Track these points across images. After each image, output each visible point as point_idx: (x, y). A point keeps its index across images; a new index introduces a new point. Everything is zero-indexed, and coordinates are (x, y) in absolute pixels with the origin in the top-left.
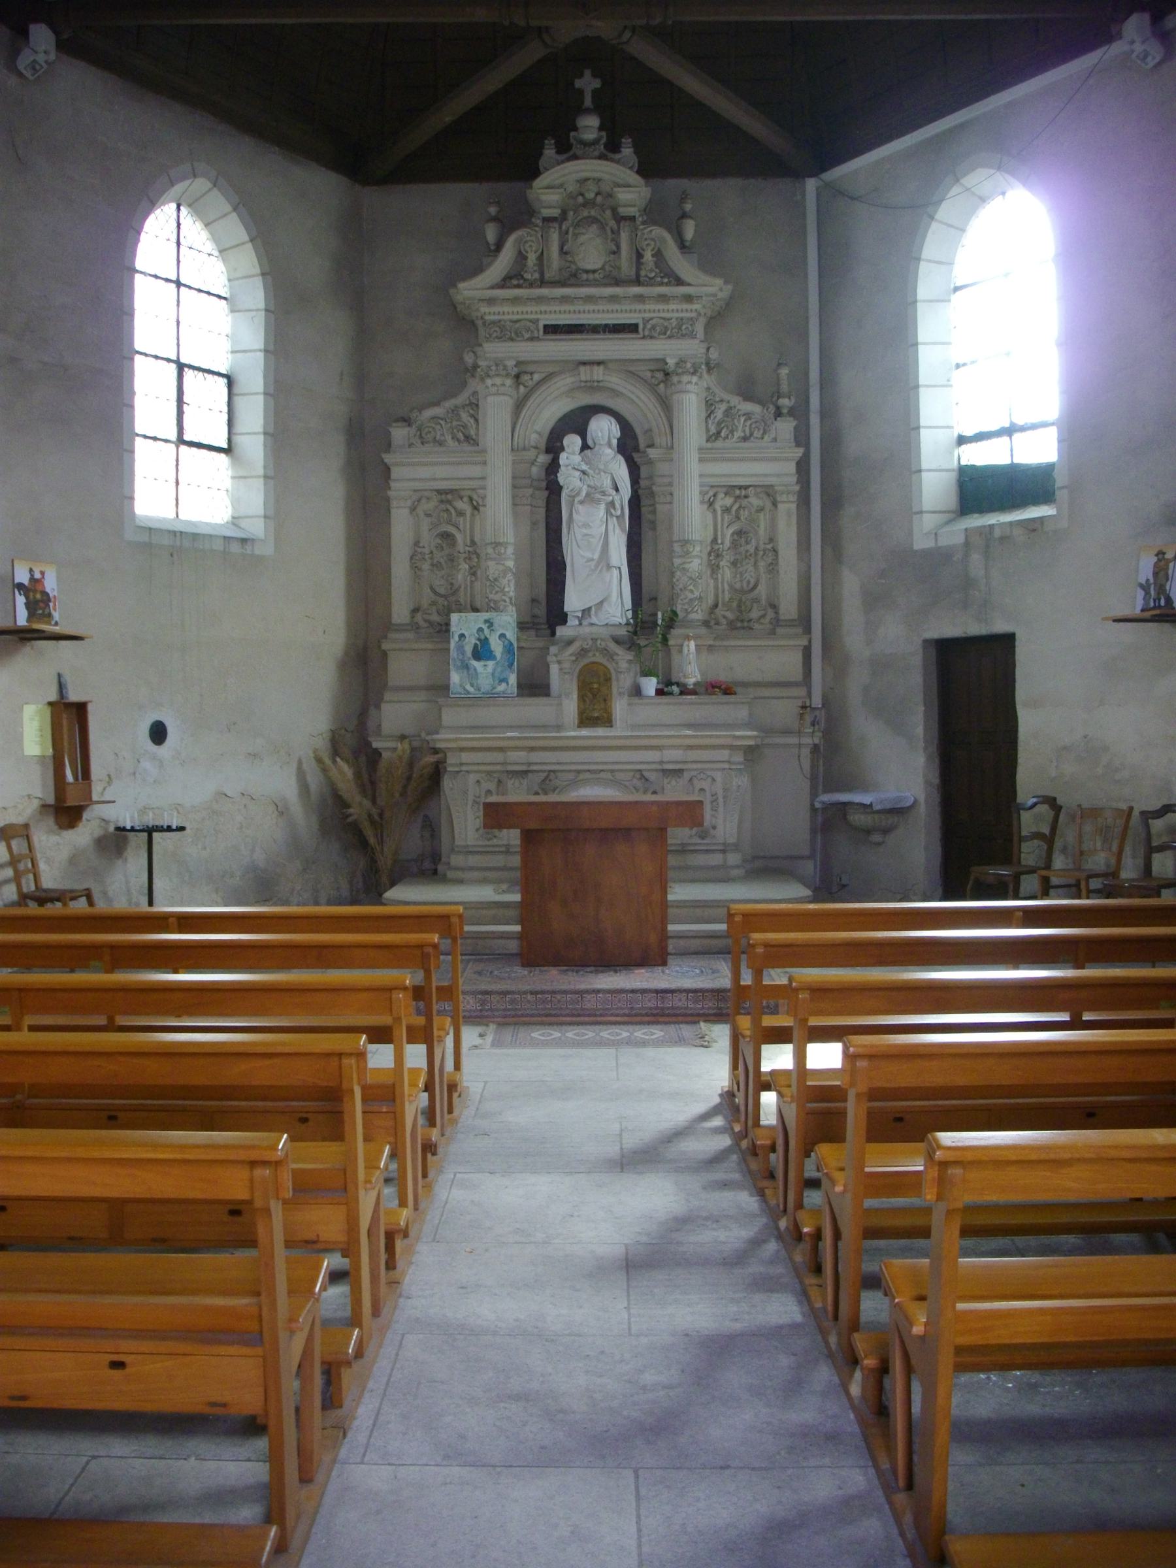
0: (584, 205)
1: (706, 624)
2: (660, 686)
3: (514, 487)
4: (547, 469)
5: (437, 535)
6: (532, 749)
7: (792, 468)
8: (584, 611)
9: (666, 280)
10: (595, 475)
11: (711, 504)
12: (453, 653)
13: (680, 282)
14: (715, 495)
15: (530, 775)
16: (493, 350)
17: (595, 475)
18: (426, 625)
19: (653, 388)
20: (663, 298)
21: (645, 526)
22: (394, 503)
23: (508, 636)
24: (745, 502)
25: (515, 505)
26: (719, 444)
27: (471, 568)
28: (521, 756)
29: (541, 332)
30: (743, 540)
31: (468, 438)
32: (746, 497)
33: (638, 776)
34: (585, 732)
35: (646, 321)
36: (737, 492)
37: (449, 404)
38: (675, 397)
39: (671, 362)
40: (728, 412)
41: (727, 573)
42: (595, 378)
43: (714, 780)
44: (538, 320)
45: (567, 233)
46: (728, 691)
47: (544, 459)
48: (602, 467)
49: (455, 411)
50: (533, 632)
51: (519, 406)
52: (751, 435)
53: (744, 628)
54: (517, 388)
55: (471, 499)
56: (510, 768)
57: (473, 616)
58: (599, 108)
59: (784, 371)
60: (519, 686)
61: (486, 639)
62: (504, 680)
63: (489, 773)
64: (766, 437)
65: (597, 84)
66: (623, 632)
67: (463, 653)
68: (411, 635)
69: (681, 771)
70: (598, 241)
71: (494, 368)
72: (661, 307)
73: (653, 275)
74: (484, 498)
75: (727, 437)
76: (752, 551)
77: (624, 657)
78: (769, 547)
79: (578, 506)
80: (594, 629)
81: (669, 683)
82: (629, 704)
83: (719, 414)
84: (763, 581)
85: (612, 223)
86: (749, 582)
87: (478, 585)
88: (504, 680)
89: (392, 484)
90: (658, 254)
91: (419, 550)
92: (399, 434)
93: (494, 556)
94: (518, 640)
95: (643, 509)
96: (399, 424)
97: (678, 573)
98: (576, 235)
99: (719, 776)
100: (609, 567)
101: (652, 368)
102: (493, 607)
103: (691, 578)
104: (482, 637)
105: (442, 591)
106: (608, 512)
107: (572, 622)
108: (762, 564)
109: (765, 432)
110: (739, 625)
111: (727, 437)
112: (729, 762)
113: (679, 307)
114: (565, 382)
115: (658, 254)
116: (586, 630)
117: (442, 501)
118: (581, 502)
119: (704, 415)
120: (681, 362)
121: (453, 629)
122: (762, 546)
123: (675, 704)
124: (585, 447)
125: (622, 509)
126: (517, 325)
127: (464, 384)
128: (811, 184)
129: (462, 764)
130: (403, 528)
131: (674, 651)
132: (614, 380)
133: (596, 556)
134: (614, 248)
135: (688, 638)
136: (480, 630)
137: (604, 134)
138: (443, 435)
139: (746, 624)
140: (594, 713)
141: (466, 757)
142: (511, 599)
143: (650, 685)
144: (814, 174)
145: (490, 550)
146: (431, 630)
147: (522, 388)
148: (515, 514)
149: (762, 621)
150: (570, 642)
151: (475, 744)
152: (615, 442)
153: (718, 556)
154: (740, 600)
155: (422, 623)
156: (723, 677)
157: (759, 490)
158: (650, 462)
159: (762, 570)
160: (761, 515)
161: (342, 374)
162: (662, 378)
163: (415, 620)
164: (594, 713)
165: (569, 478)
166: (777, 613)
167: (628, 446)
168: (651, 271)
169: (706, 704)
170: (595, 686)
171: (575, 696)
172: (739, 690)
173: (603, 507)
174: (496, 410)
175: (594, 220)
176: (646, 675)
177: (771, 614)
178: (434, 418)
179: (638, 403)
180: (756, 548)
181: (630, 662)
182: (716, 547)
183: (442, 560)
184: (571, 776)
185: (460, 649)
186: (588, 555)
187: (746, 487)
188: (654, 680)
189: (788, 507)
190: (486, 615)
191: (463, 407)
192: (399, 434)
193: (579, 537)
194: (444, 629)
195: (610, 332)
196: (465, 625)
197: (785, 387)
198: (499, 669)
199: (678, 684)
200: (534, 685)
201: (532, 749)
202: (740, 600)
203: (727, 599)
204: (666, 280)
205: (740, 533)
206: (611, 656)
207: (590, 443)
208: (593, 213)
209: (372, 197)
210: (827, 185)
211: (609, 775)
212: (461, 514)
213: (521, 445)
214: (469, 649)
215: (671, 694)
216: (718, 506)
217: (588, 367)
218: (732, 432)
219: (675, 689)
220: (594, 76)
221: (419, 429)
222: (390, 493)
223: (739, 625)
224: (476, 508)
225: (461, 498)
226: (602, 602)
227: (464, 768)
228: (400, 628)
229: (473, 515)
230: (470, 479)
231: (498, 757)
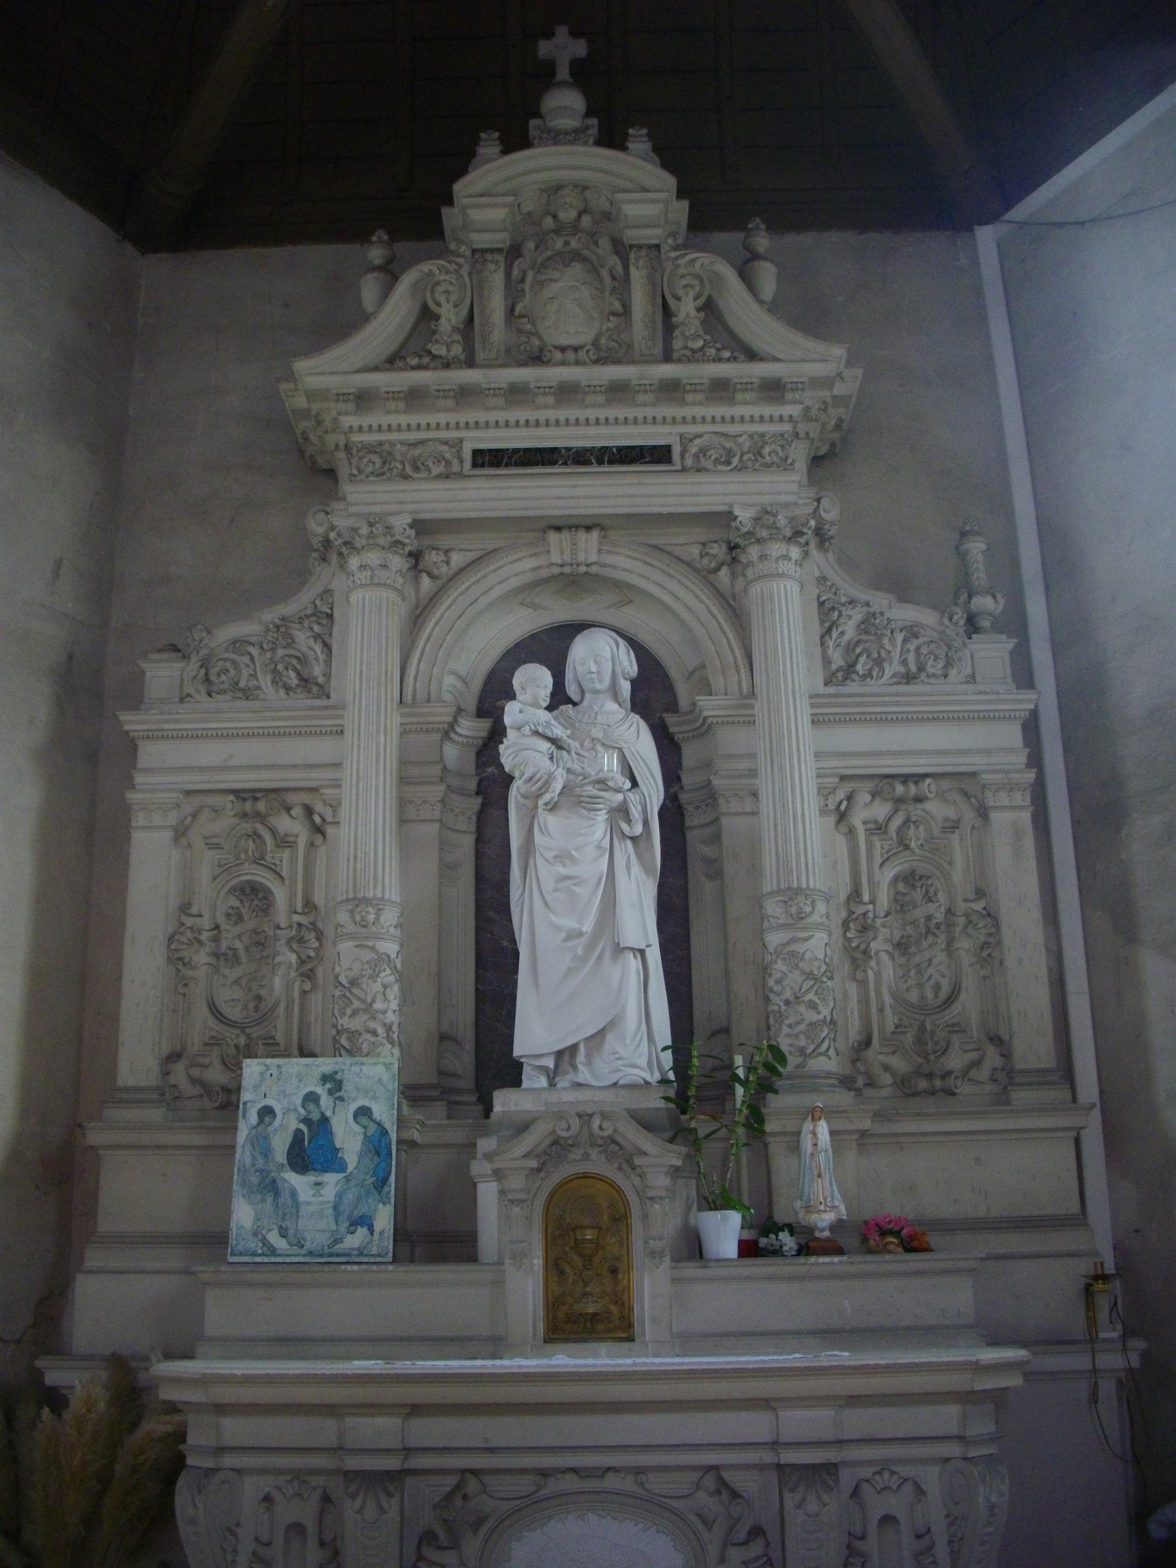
0: (557, 232)
1: (846, 1082)
2: (748, 1235)
3: (403, 780)
4: (479, 754)
5: (233, 890)
6: (415, 1410)
7: (1013, 735)
8: (559, 1054)
9: (727, 354)
10: (583, 767)
11: (842, 817)
12: (243, 1154)
13: (752, 355)
14: (850, 798)
15: (409, 1481)
16: (364, 497)
17: (583, 767)
18: (197, 1091)
19: (706, 576)
20: (721, 389)
21: (696, 869)
22: (140, 819)
23: (377, 1115)
24: (916, 811)
25: (403, 821)
26: (852, 687)
27: (302, 962)
28: (380, 1429)
29: (468, 464)
30: (918, 895)
31: (306, 682)
32: (919, 799)
33: (710, 1482)
34: (563, 1359)
35: (685, 440)
36: (900, 789)
37: (271, 615)
38: (755, 590)
39: (744, 516)
40: (867, 625)
41: (885, 968)
42: (581, 557)
43: (919, 1491)
44: (461, 441)
45: (523, 280)
46: (913, 1244)
47: (471, 728)
48: (597, 733)
49: (282, 628)
50: (441, 1108)
51: (417, 618)
52: (921, 668)
53: (933, 1092)
54: (416, 580)
55: (309, 811)
56: (353, 1463)
57: (295, 1065)
58: (582, 75)
59: (976, 547)
60: (401, 1235)
61: (325, 1120)
62: (364, 1221)
63: (298, 1475)
64: (953, 672)
65: (580, 49)
66: (654, 1102)
67: (267, 1152)
68: (155, 1114)
69: (831, 1469)
70: (585, 292)
71: (364, 530)
72: (719, 411)
73: (700, 343)
74: (335, 807)
75: (869, 674)
76: (940, 917)
77: (660, 1157)
78: (978, 906)
79: (543, 815)
80: (586, 1095)
81: (770, 1227)
82: (675, 1280)
83: (849, 628)
84: (970, 981)
85: (614, 261)
86: (937, 987)
87: (316, 999)
88: (364, 1221)
89: (139, 779)
90: (709, 308)
91: (189, 922)
92: (161, 675)
93: (352, 928)
94: (401, 1122)
95: (691, 836)
96: (166, 656)
97: (780, 966)
98: (540, 284)
99: (931, 1478)
100: (619, 950)
101: (703, 538)
102: (345, 1045)
103: (809, 976)
104: (315, 1116)
105: (235, 1013)
106: (614, 831)
107: (533, 1080)
108: (964, 945)
109: (948, 664)
110: (923, 1084)
111: (869, 674)
112: (961, 1438)
113: (756, 411)
114: (519, 566)
115: (709, 308)
116: (565, 1096)
117: (245, 815)
118: (553, 807)
119: (817, 630)
120: (765, 515)
121: (246, 1096)
122: (961, 907)
123: (790, 1278)
124: (559, 698)
125: (646, 823)
126: (417, 452)
127: (303, 576)
128: (986, 237)
129: (221, 1450)
130: (156, 873)
131: (777, 1148)
132: (625, 563)
133: (588, 927)
134: (617, 306)
135: (813, 1114)
136: (311, 1098)
137: (593, 122)
138: (254, 676)
139: (938, 1083)
140: (587, 1304)
141: (234, 1429)
142: (388, 1028)
143: (725, 1231)
144: (992, 218)
145: (343, 917)
146: (206, 1103)
147: (425, 581)
148: (405, 844)
149: (973, 1074)
150: (523, 1127)
151: (262, 1394)
152: (626, 687)
153: (864, 929)
154: (922, 1028)
155: (187, 1089)
156: (893, 1207)
157: (945, 784)
158: (705, 730)
159: (966, 959)
160: (955, 838)
161: (58, 564)
162: (725, 551)
163: (172, 1080)
164: (587, 1304)
165: (522, 753)
166: (1007, 1055)
167: (653, 694)
168: (696, 337)
169: (867, 1276)
170: (589, 1235)
171: (538, 1262)
172: (933, 1239)
173: (602, 816)
174: (368, 610)
175: (577, 257)
176: (714, 1206)
177: (992, 1058)
178: (237, 644)
179: (678, 617)
180: (949, 911)
181: (675, 1172)
182: (860, 910)
183: (238, 945)
184: (525, 1485)
185: (261, 1143)
186: (571, 923)
187: (919, 778)
188: (734, 1218)
189: (1011, 817)
190: (326, 1064)
191: (301, 620)
192: (161, 675)
193: (548, 883)
194: (228, 1101)
195: (611, 462)
196: (275, 1087)
197: (980, 576)
198: (351, 1196)
199: (791, 1228)
200: (436, 1235)
201: (415, 1410)
202: (922, 1028)
203: (890, 1027)
204: (727, 354)
205: (910, 878)
206: (628, 1159)
207: (572, 690)
208: (574, 244)
209: (158, 273)
210: (1023, 225)
211: (628, 1484)
212: (284, 842)
213: (421, 695)
214: (280, 1144)
215: (776, 1252)
216: (857, 819)
217: (566, 535)
218: (879, 662)
219: (787, 1241)
220: (573, 34)
221: (205, 664)
222: (132, 796)
223: (923, 1084)
224: (319, 830)
225: (288, 810)
226: (601, 1034)
227: (228, 1461)
228: (135, 1097)
229: (312, 845)
230: (311, 766)
231: (324, 1431)
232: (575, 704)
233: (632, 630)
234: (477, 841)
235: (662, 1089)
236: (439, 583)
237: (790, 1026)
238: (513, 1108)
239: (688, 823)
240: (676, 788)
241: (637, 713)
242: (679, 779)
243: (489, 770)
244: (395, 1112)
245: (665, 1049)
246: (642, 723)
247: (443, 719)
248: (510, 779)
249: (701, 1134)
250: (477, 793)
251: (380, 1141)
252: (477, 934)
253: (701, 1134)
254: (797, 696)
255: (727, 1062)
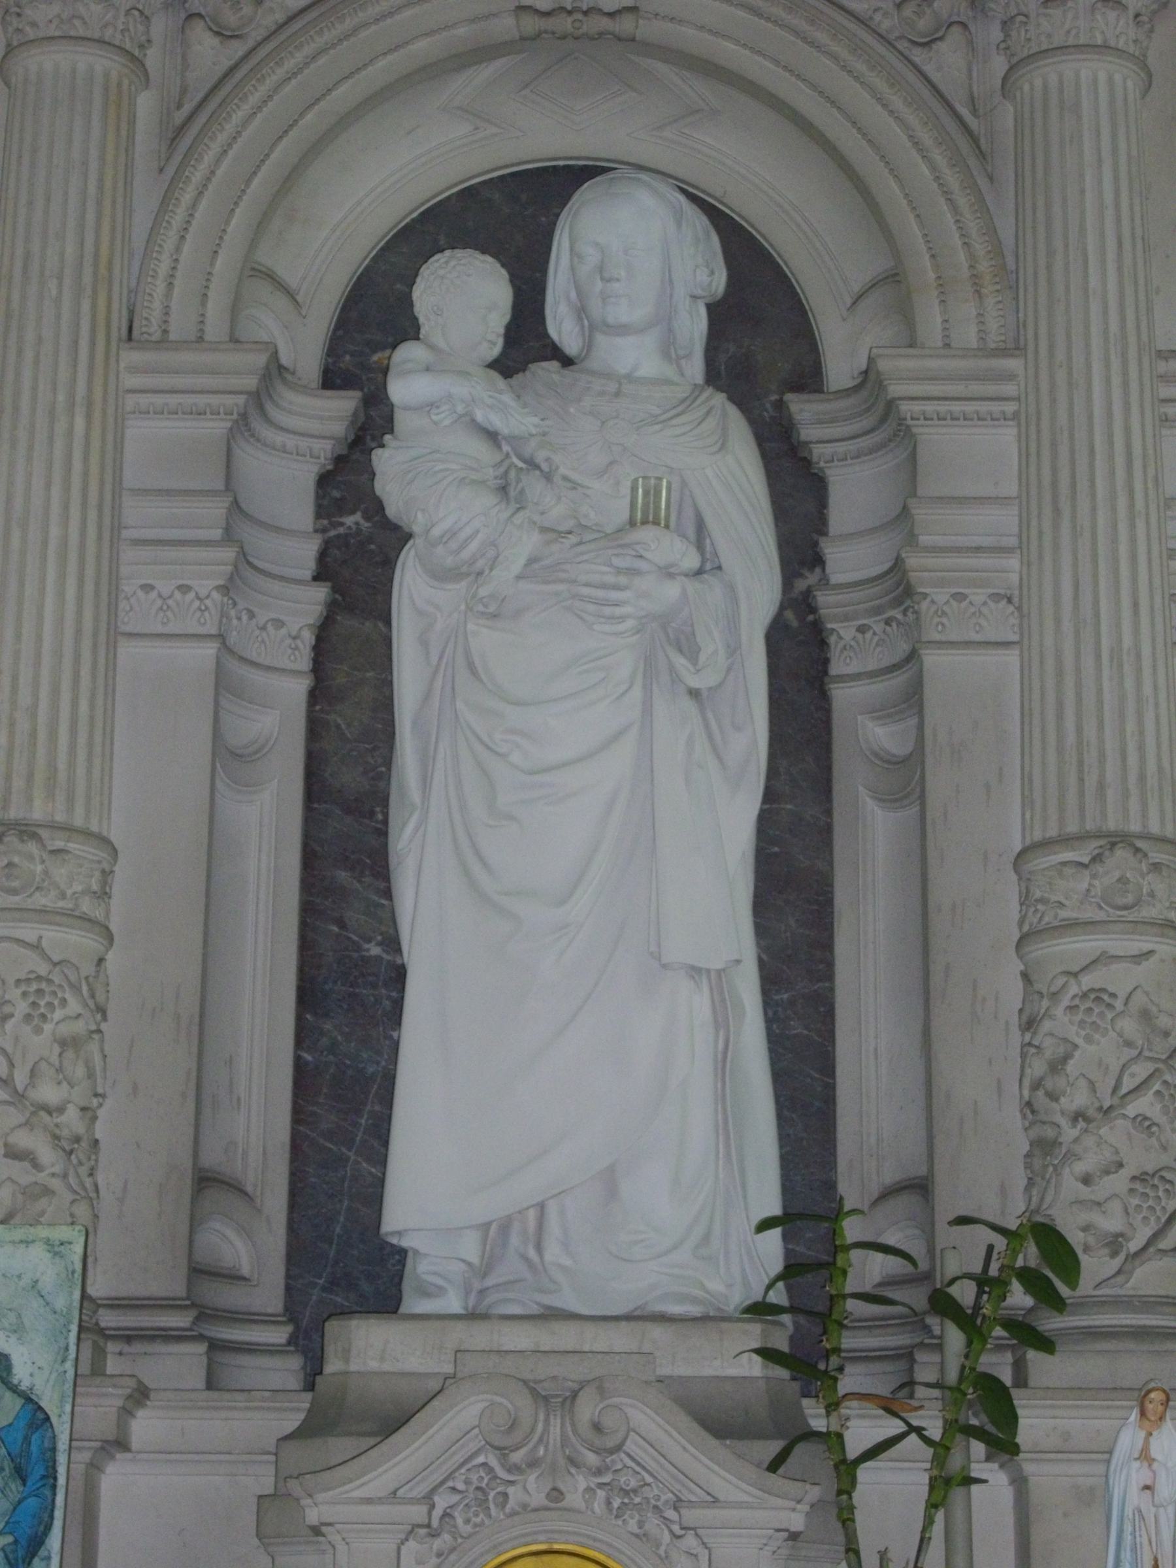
23: (21, 1373)
66: (735, 1361)
95: (843, 696)
124: (526, 344)
165: (429, 478)
167: (757, 339)
207: (561, 325)
232: (567, 362)
233: (714, 185)
234: (314, 696)
235: (756, 1328)
236: (238, 49)
237: (1086, 1180)
238: (374, 1365)
239: (835, 669)
240: (812, 578)
241: (719, 389)
242: (818, 561)
243: (350, 520)
244: (69, 1365)
245: (765, 1225)
246: (733, 412)
247: (235, 382)
248: (399, 536)
249: (855, 1444)
250: (317, 578)
251: (27, 1440)
252: (304, 925)
253: (855, 1444)
254: (1132, 352)
255: (923, 1266)
